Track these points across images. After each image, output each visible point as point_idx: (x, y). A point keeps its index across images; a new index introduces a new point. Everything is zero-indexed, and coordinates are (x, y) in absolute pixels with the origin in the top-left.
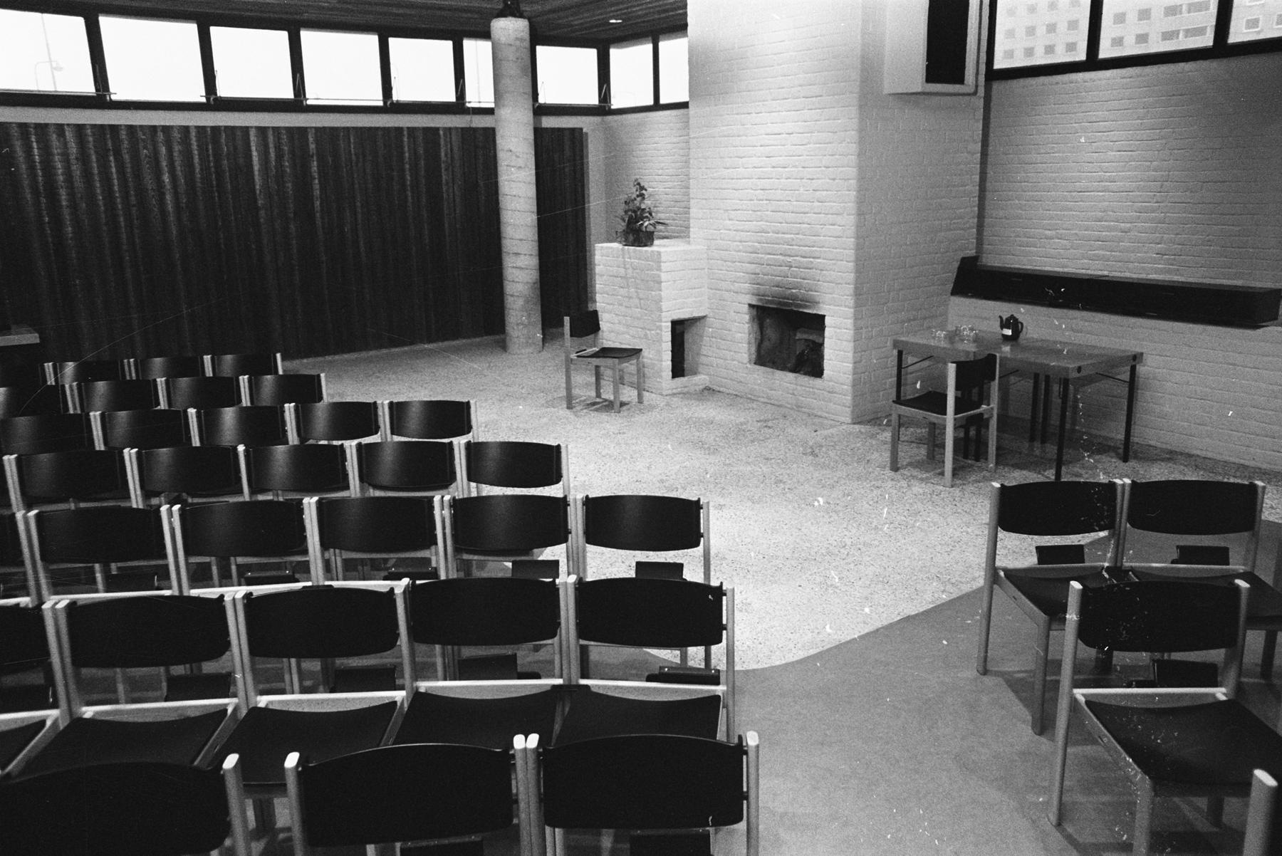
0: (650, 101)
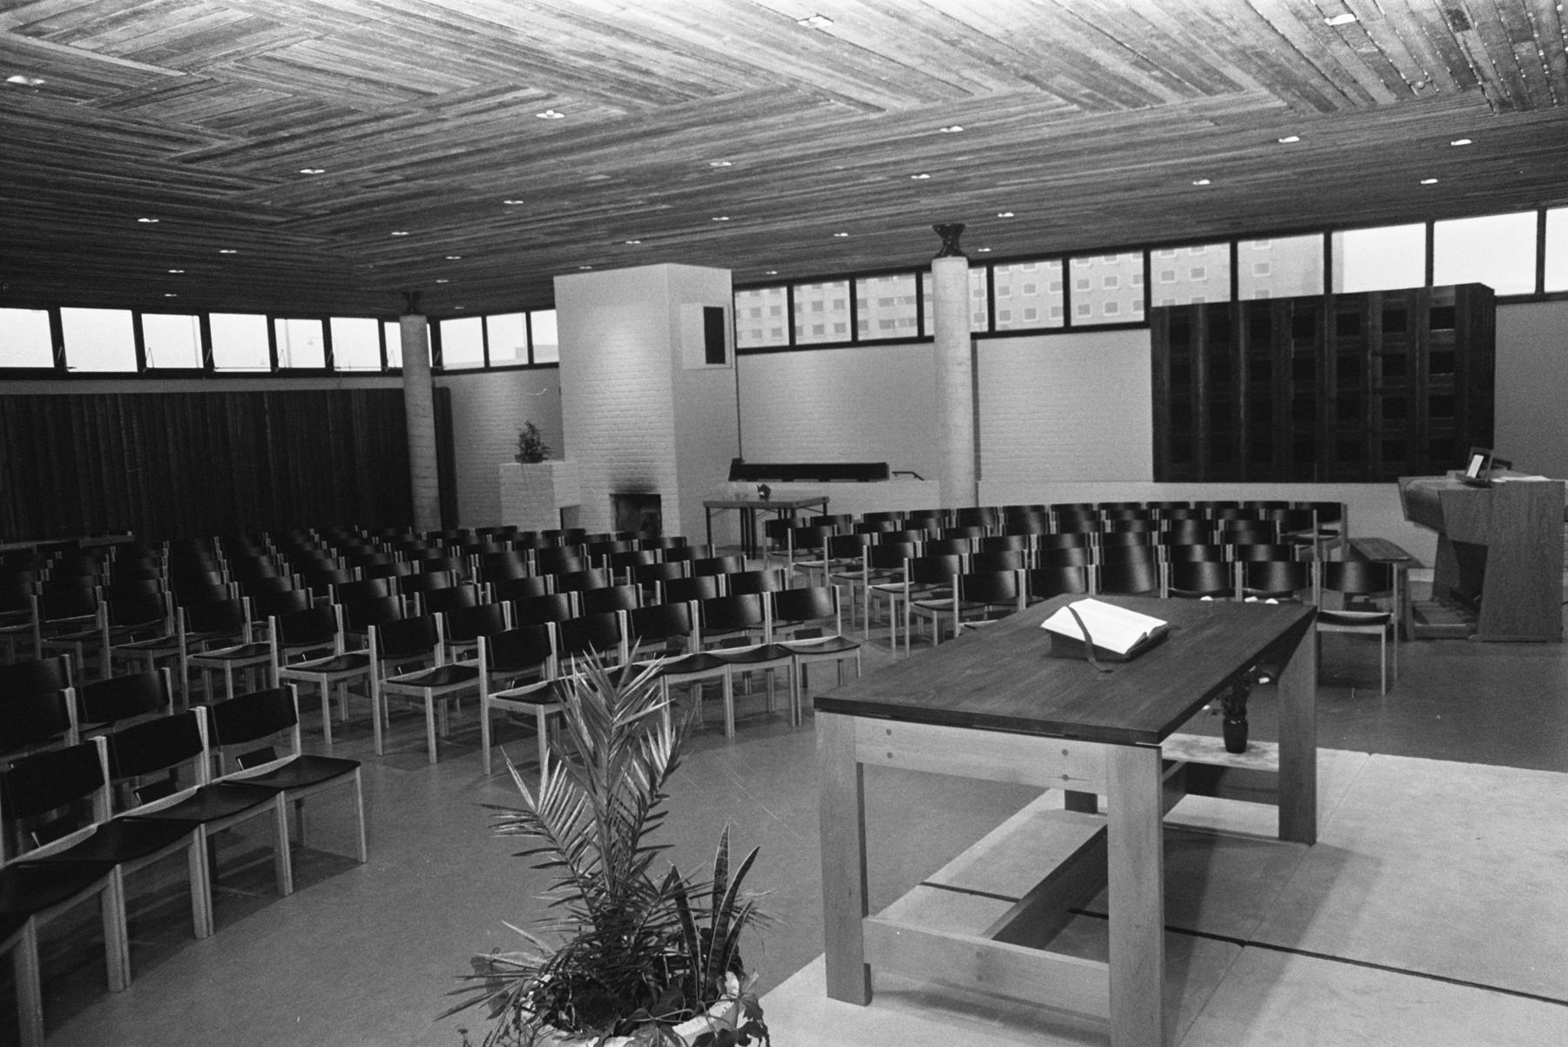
0: (482, 365)
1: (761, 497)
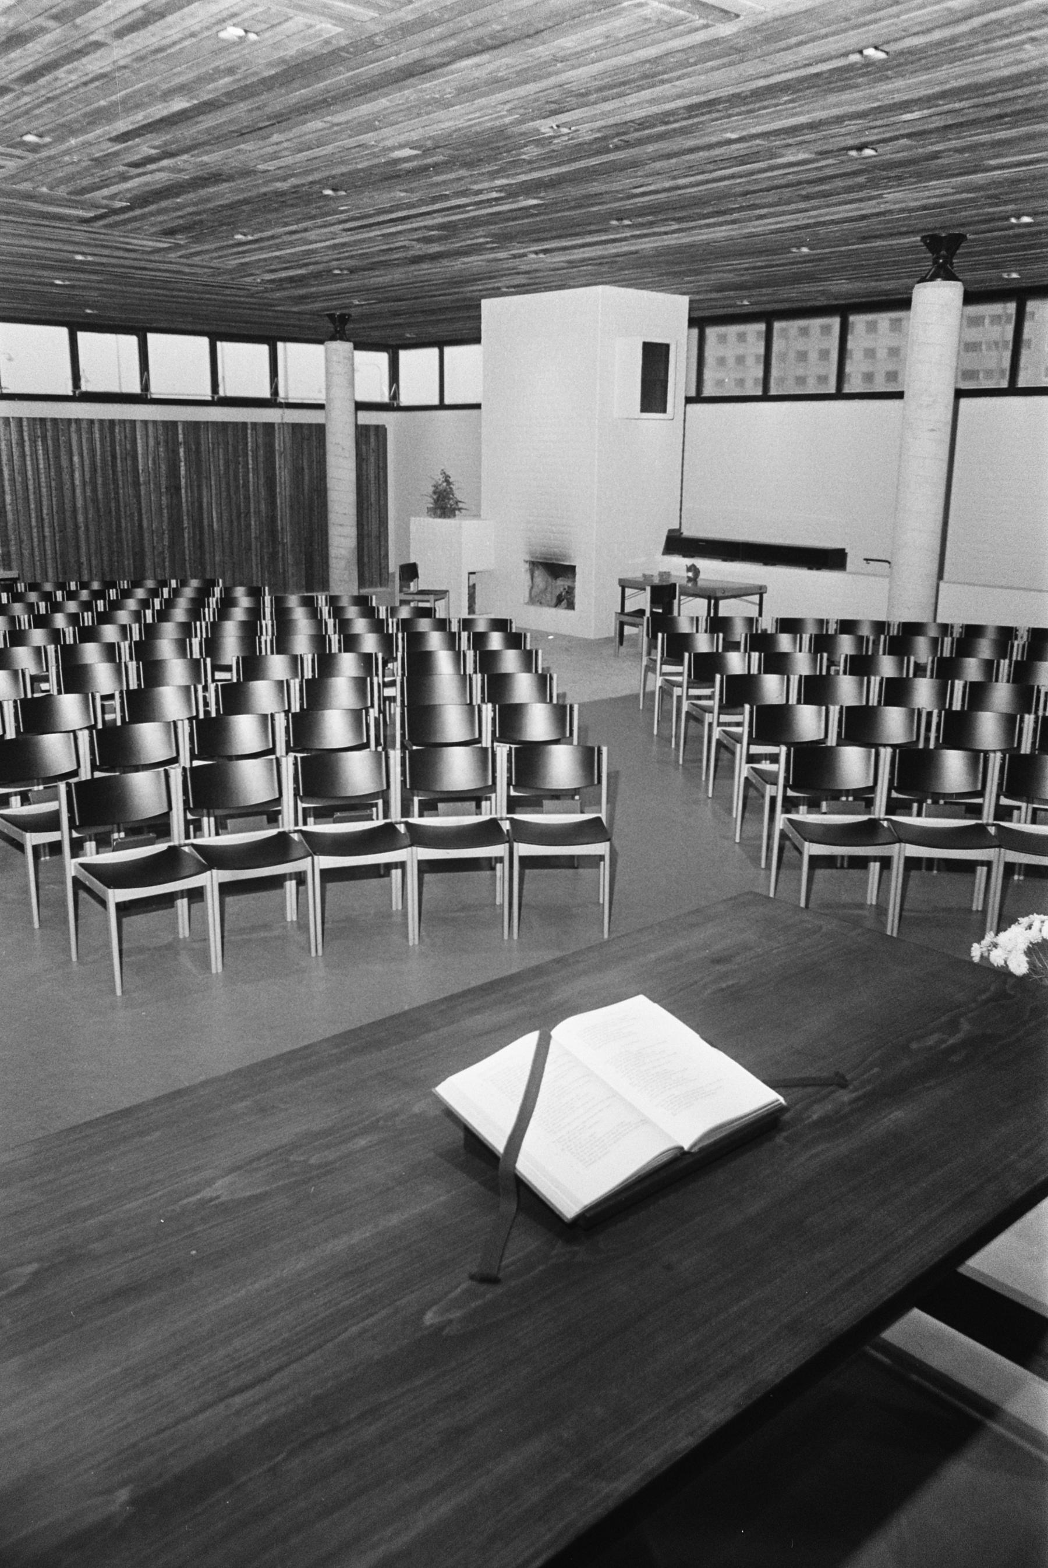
0: (436, 402)
1: (689, 579)
